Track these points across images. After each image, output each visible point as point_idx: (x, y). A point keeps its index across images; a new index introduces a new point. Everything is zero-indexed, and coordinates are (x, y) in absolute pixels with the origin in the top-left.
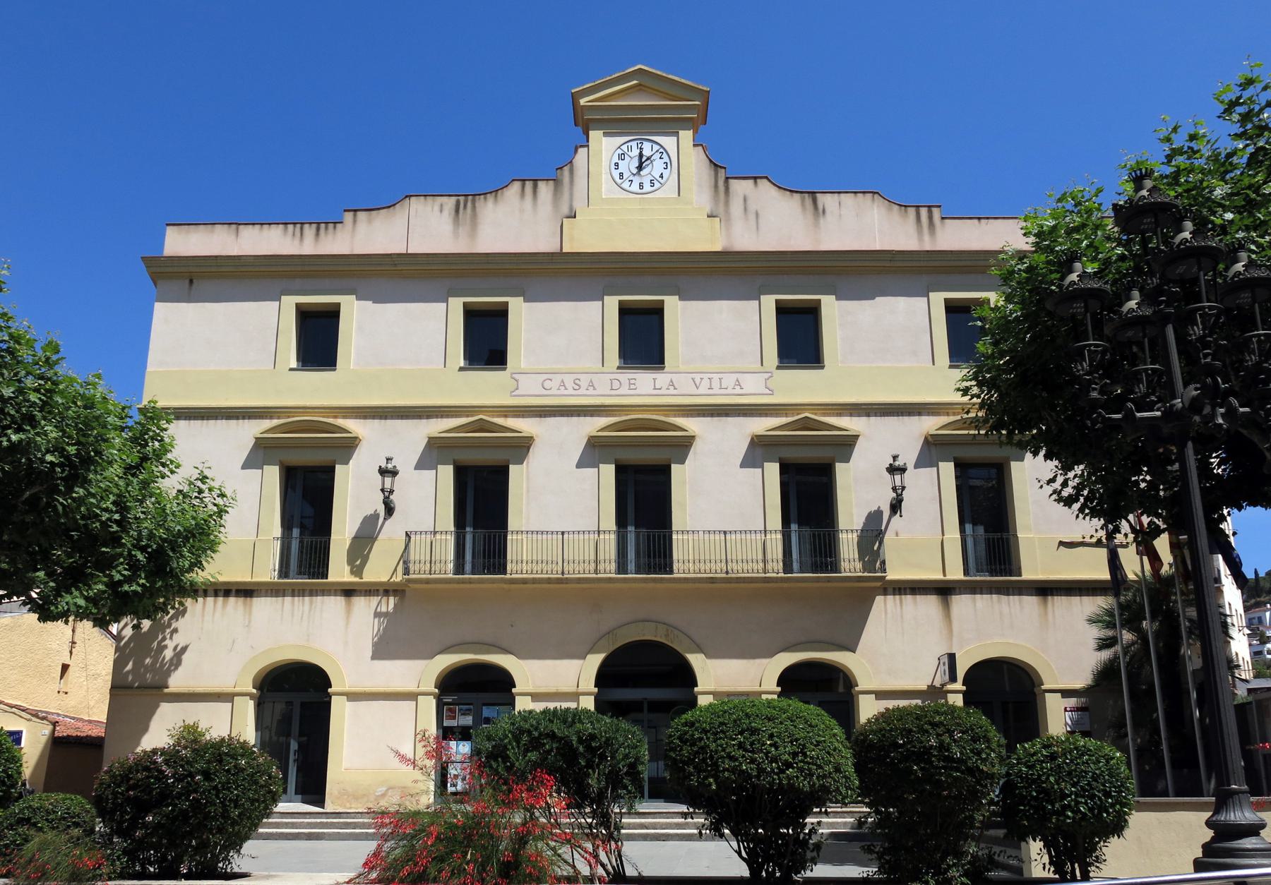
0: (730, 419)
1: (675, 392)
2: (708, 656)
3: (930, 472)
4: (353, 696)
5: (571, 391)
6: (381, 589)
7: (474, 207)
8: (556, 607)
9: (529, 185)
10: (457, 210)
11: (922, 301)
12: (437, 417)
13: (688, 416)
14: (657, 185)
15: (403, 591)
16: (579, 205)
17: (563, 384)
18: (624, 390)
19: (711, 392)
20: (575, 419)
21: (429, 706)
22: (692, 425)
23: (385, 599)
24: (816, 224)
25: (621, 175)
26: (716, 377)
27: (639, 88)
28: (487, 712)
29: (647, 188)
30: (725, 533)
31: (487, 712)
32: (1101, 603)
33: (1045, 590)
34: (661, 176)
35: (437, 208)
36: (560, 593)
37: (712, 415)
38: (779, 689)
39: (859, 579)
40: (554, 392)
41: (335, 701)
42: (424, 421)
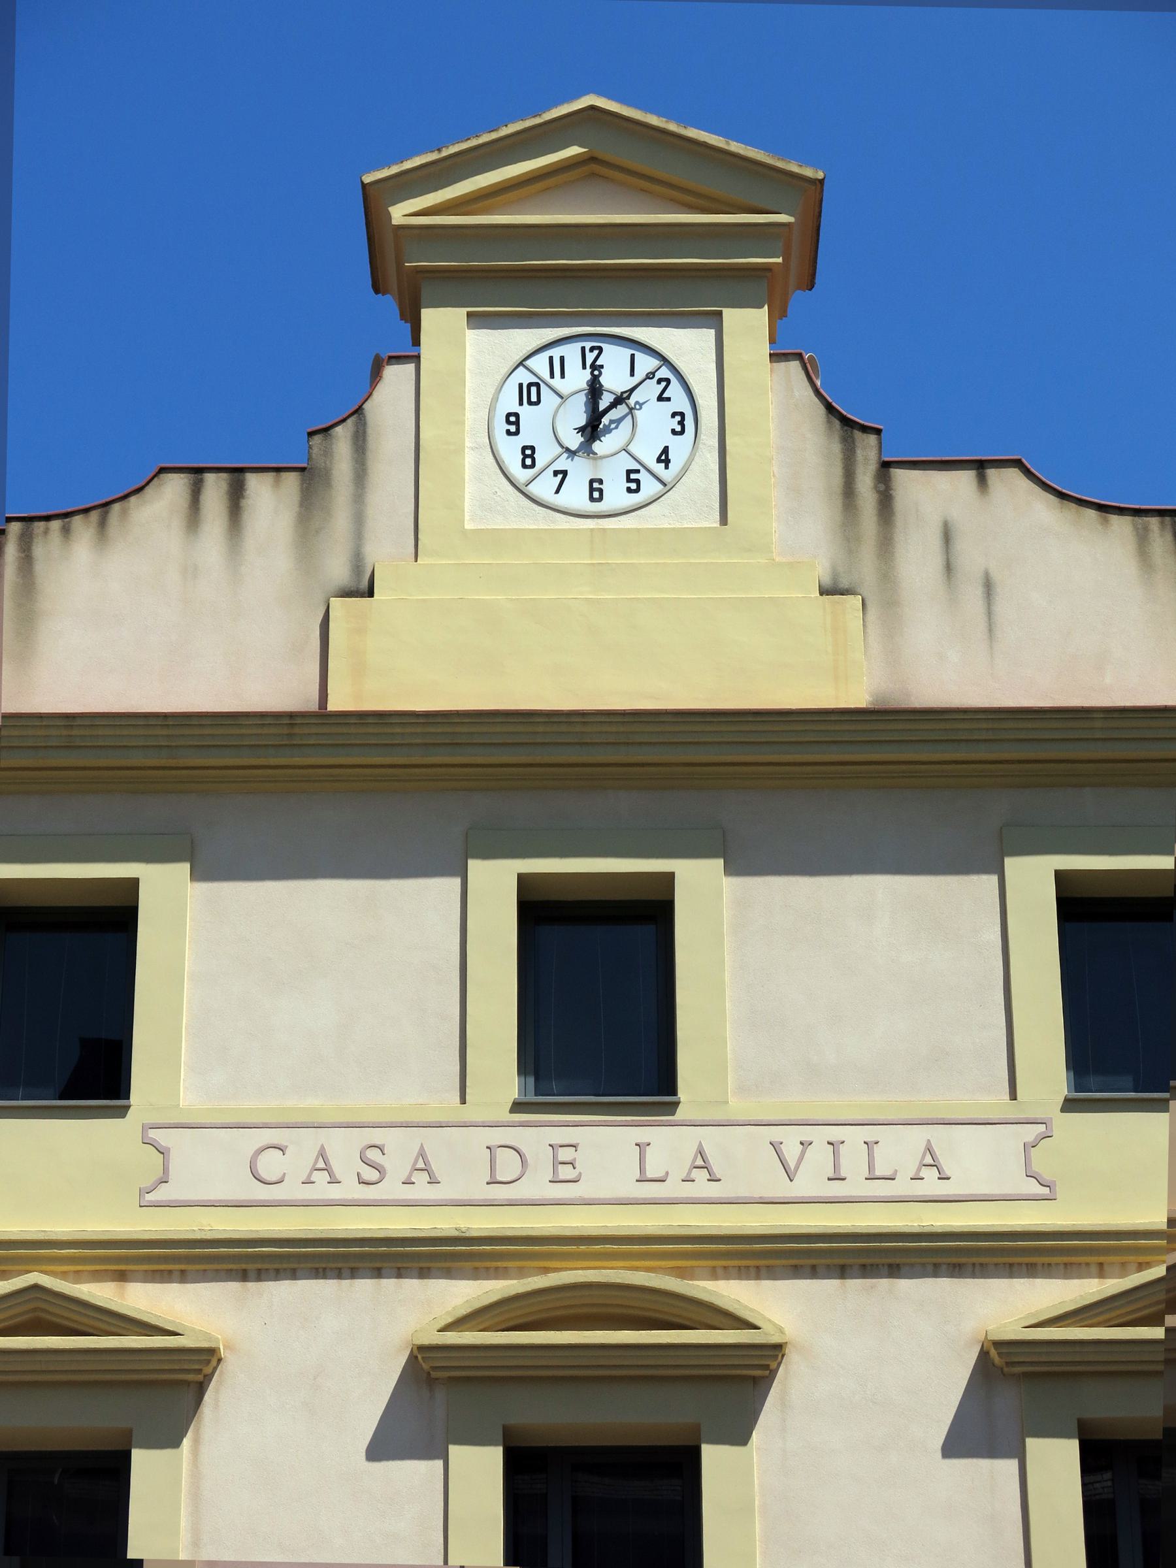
5: (350, 1189)
9: (215, 487)
16: (384, 550)
18: (536, 1186)
22: (773, 1306)
25: (528, 454)
34: (664, 458)
37: (842, 1272)
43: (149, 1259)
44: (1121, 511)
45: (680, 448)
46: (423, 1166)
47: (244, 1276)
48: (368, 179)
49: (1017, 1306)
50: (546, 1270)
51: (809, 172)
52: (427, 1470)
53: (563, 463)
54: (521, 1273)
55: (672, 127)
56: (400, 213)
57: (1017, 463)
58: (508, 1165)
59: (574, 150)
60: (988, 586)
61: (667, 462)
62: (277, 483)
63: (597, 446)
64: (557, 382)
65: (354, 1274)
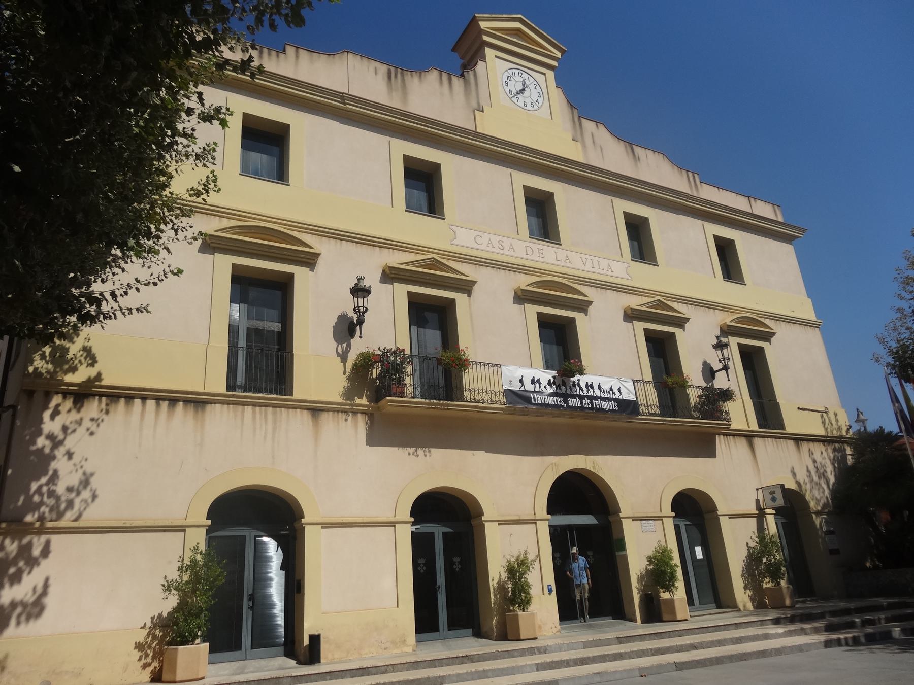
7: (403, 80)
10: (389, 77)
11: (390, 286)
14: (536, 107)
16: (484, 103)
17: (490, 242)
18: (535, 257)
29: (529, 107)
35: (372, 70)
40: (483, 247)
41: (308, 530)
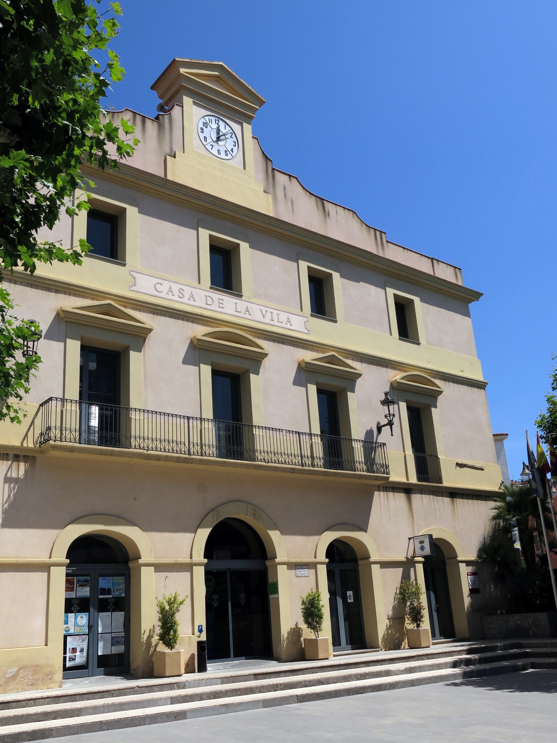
0: (285, 346)
1: (249, 317)
2: (283, 533)
3: (193, 369)
4: (159, 568)
5: (176, 298)
6: (11, 453)
8: (165, 485)
9: (139, 119)
12: (65, 293)
13: (140, 310)
15: (34, 458)
16: (177, 149)
18: (215, 307)
19: (272, 323)
20: (180, 322)
21: (59, 575)
22: (266, 346)
23: (15, 464)
24: (325, 221)
25: (205, 138)
26: (275, 312)
27: (216, 79)
28: (103, 583)
30: (188, 418)
31: (103, 583)
32: (20, 470)
33: (455, 494)
34: (232, 150)
36: (170, 471)
37: (274, 341)
38: (68, 561)
39: (72, 450)
42: (53, 294)
43: (132, 304)
44: (313, 195)
45: (235, 149)
46: (192, 296)
47: (154, 313)
48: (177, 59)
49: (309, 356)
50: (218, 327)
51: (263, 99)
52: (195, 369)
53: (212, 143)
54: (213, 327)
55: (238, 77)
56: (182, 70)
57: (296, 178)
58: (210, 301)
59: (217, 73)
60: (292, 202)
61: (233, 152)
62: (153, 123)
63: (219, 142)
64: (210, 124)
65: (178, 318)
